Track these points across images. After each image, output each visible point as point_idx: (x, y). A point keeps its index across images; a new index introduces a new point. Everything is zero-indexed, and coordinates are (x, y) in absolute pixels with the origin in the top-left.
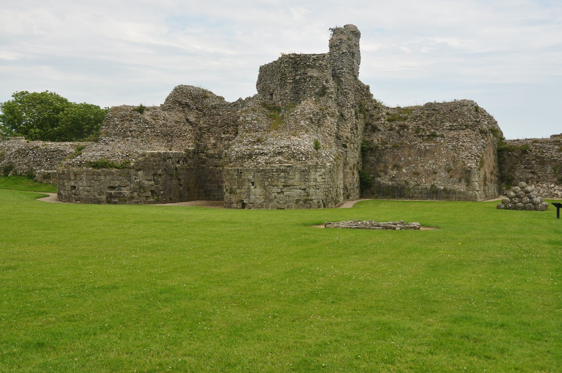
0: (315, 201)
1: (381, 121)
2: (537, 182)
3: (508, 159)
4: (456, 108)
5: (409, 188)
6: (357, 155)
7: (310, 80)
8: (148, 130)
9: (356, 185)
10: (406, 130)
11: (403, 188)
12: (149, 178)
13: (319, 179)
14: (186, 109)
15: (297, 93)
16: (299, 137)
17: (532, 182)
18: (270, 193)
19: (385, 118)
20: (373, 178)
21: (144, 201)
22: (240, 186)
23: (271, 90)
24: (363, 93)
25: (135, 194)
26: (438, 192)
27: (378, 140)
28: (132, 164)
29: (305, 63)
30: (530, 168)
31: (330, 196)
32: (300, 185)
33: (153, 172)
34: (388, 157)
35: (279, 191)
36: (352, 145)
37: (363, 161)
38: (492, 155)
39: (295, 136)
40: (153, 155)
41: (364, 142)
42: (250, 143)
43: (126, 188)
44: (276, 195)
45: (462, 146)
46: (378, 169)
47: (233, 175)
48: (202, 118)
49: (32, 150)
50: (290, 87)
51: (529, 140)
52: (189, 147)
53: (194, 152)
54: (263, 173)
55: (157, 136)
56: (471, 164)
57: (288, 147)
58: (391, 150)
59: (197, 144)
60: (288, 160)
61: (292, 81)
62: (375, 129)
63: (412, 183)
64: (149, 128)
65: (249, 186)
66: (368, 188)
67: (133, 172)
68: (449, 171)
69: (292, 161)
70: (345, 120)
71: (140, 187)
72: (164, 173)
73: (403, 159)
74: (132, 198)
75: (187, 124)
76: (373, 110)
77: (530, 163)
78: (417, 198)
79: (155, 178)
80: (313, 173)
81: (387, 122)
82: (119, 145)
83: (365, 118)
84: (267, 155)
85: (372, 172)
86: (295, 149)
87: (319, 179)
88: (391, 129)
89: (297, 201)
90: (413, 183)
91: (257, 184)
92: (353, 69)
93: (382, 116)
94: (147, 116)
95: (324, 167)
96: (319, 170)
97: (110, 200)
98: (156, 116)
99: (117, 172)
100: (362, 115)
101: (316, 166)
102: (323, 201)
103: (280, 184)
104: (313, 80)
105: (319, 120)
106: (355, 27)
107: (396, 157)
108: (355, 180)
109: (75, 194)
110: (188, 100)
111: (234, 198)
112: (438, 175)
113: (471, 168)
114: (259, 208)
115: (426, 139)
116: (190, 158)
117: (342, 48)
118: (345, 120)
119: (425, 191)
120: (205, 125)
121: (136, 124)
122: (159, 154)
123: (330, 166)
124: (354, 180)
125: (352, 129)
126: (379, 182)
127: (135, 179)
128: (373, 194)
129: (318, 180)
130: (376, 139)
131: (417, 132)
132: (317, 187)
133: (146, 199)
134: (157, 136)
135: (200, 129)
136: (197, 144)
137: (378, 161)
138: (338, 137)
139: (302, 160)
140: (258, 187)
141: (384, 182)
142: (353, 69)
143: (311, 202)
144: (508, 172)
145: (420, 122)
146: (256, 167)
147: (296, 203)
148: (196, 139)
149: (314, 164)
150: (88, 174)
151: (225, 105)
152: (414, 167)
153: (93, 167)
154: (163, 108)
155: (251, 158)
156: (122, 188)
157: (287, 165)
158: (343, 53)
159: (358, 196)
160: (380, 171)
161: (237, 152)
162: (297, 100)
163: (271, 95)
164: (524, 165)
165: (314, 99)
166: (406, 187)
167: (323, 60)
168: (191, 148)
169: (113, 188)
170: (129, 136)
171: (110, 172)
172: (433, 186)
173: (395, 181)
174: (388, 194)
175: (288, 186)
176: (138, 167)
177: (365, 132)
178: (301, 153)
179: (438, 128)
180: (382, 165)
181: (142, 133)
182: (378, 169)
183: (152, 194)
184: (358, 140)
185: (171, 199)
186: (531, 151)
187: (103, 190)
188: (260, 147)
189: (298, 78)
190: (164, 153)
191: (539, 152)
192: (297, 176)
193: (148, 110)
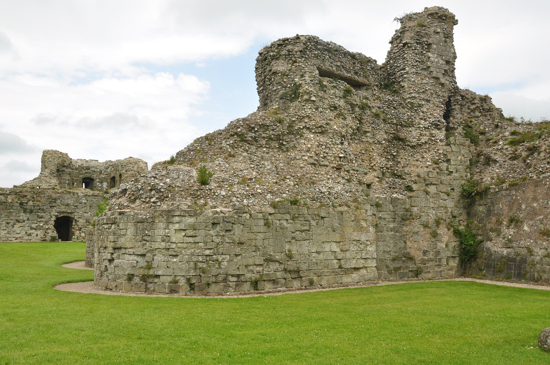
5: (533, 261)
10: (536, 155)
11: (524, 261)
20: (482, 241)
34: (502, 206)
46: (489, 226)
58: (508, 192)
66: (470, 257)
73: (523, 206)
76: (493, 131)
89: (130, 277)
90: (541, 252)
104: (278, 78)
107: (513, 204)
126: (488, 249)
141: (496, 249)
143: (156, 280)
152: (541, 221)
160: (491, 230)
166: (529, 259)
173: (512, 247)
174: (500, 271)
180: (494, 219)
182: (489, 226)
192: (131, 231)
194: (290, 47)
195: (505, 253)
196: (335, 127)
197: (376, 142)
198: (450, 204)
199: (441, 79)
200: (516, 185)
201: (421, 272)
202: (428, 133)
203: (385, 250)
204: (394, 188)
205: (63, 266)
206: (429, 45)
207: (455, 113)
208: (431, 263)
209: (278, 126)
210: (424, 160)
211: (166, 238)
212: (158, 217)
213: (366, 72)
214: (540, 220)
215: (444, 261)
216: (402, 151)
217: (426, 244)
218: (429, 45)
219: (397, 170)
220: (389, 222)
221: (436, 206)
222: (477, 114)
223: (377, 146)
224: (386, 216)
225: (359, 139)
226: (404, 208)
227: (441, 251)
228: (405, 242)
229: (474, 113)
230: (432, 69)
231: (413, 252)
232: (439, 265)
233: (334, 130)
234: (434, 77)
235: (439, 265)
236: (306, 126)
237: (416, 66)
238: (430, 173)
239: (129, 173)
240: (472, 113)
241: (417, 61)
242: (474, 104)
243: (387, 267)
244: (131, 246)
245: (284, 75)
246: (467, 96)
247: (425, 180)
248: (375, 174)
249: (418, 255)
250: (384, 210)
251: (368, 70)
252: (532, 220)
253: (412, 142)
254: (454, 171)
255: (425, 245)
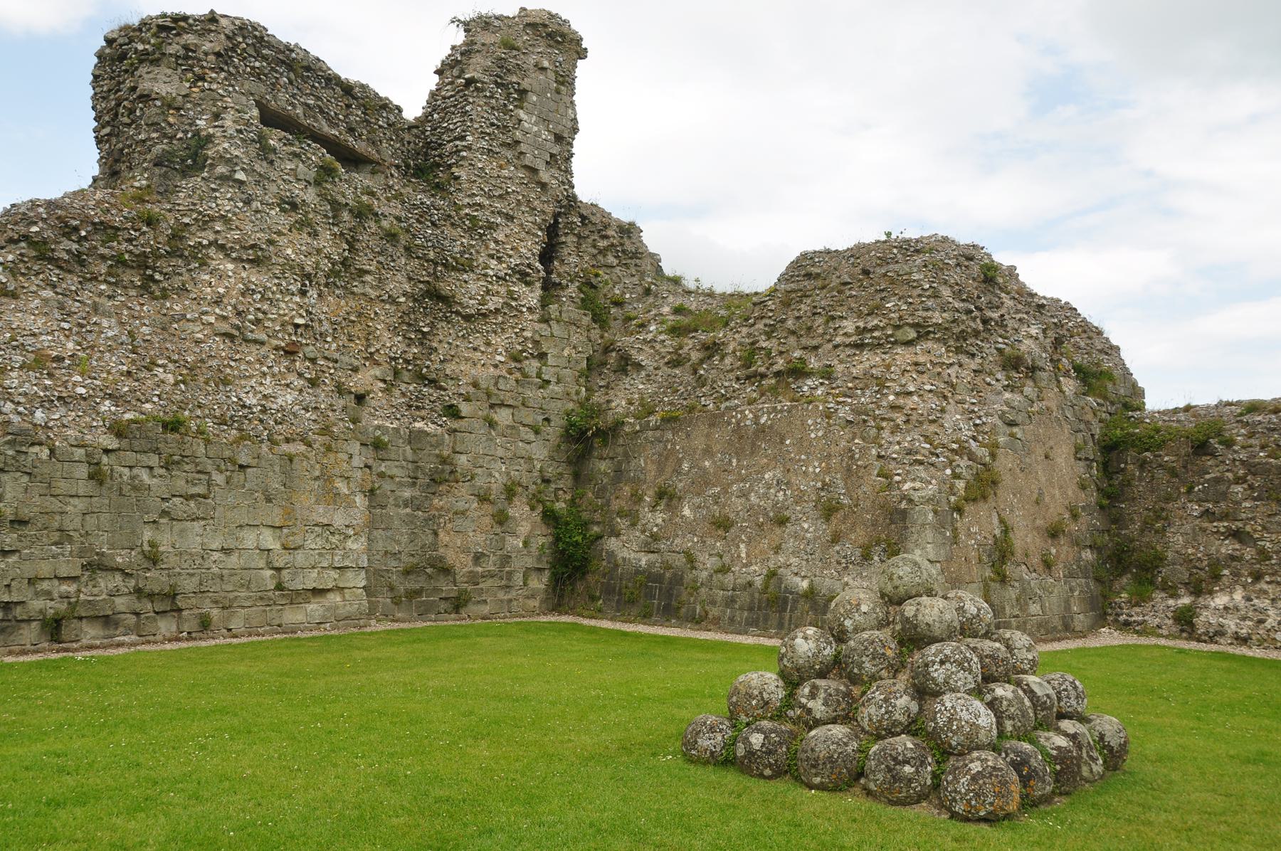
2: (1258, 577)
3: (1140, 479)
4: (884, 261)
11: (678, 580)
17: (1236, 574)
26: (785, 600)
30: (1225, 517)
34: (644, 463)
38: (1063, 455)
45: (893, 407)
51: (1229, 404)
56: (920, 486)
58: (658, 433)
66: (573, 571)
68: (829, 511)
73: (686, 466)
77: (1224, 496)
90: (711, 562)
104: (152, 112)
112: (790, 528)
113: (910, 501)
115: (773, 389)
119: (744, 598)
126: (611, 554)
130: (621, 400)
131: (748, 363)
141: (626, 555)
144: (1142, 531)
164: (1200, 501)
166: (688, 577)
172: (772, 574)
179: (815, 343)
180: (627, 490)
186: (1229, 444)
191: (1263, 447)
194: (190, 39)
195: (643, 563)
196: (289, 251)
197: (386, 297)
198: (539, 452)
199: (541, 174)
201: (467, 602)
202: (503, 290)
203: (389, 549)
204: (418, 408)
206: (523, 93)
207: (565, 251)
208: (490, 582)
209: (144, 233)
210: (490, 350)
213: (374, 131)
215: (518, 579)
216: (444, 324)
217: (480, 538)
218: (523, 93)
219: (428, 367)
220: (401, 484)
221: (510, 454)
222: (611, 259)
223: (387, 306)
224: (395, 471)
225: (345, 288)
226: (437, 456)
227: (513, 555)
228: (436, 534)
229: (605, 256)
230: (523, 147)
231: (451, 557)
232: (508, 587)
233: (287, 258)
234: (526, 167)
235: (508, 587)
236: (216, 241)
237: (489, 134)
238: (501, 380)
240: (600, 257)
241: (493, 125)
242: (606, 237)
243: (392, 589)
246: (593, 219)
247: (489, 395)
248: (377, 372)
249: (462, 564)
250: (393, 456)
251: (380, 127)
253: (468, 307)
254: (553, 380)
255: (478, 540)
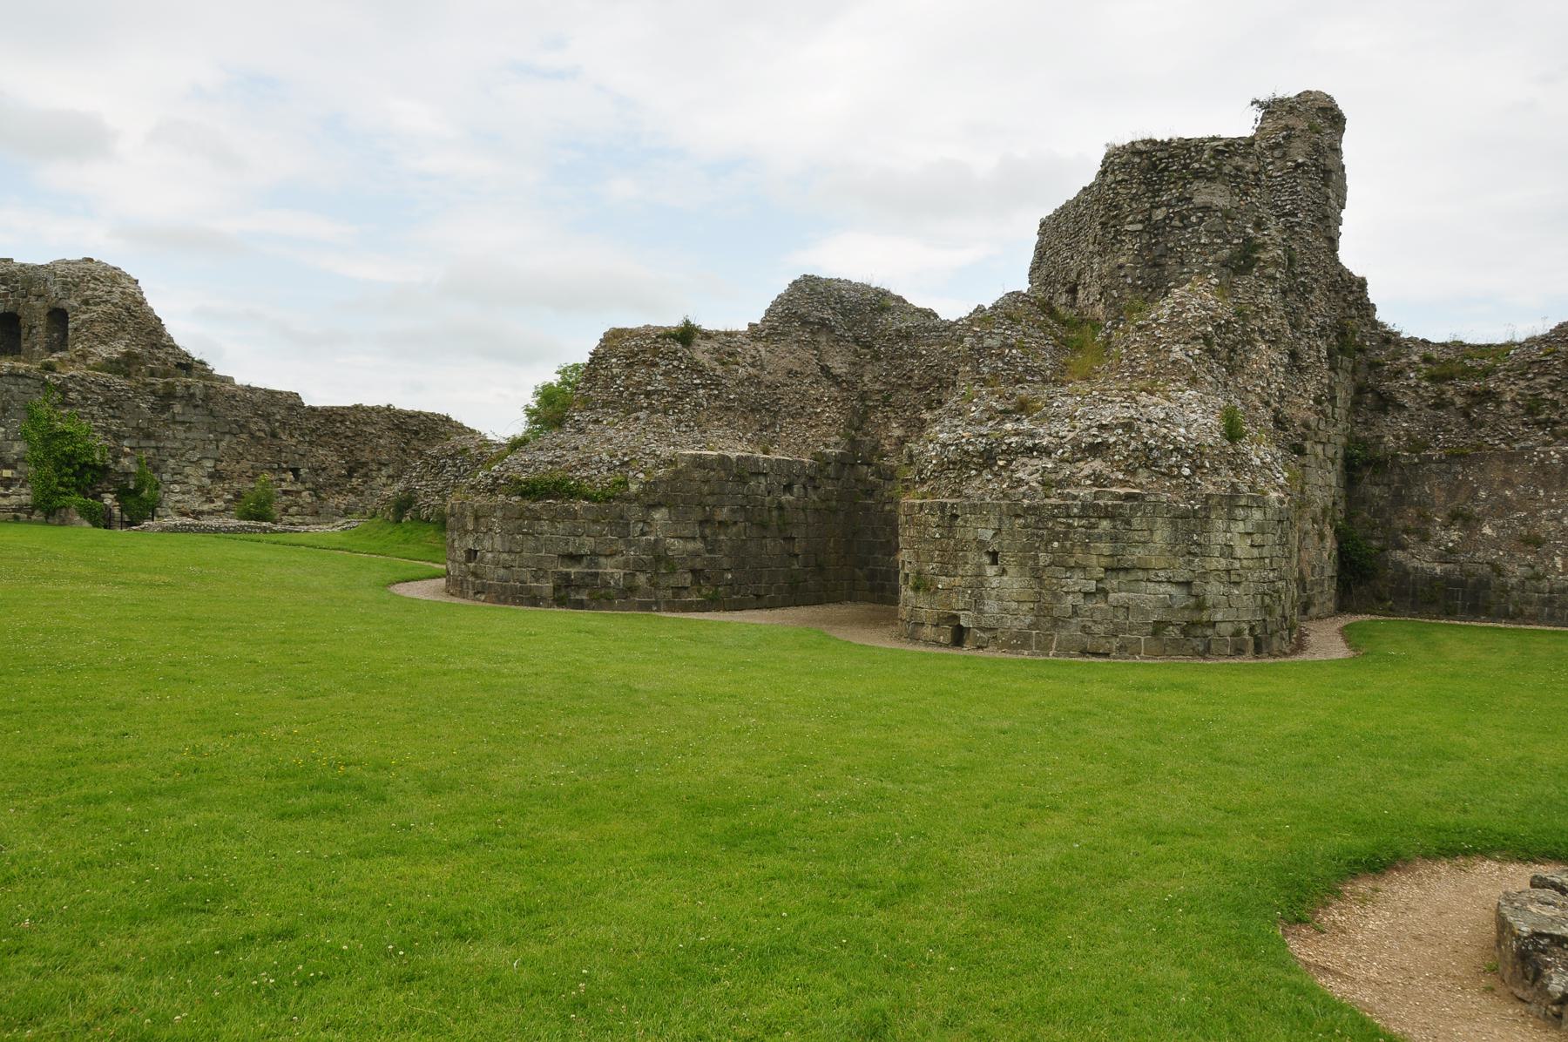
0: (1226, 629)
1: (1408, 378)
5: (1504, 585)
6: (1333, 479)
7: (1201, 220)
8: (701, 391)
9: (1329, 571)
10: (1490, 406)
11: (1483, 584)
12: (686, 533)
13: (1242, 548)
14: (823, 339)
15: (1156, 265)
16: (1168, 399)
18: (1055, 594)
19: (1419, 370)
20: (1383, 550)
21: (667, 603)
22: (950, 560)
23: (1074, 275)
24: (1350, 298)
25: (641, 579)
27: (1398, 438)
28: (634, 488)
29: (1186, 166)
31: (1279, 611)
32: (1171, 567)
33: (697, 514)
34: (1432, 489)
35: (1092, 586)
36: (1319, 448)
37: (1349, 499)
39: (1152, 393)
40: (699, 463)
41: (1353, 441)
42: (992, 414)
43: (611, 561)
44: (1080, 600)
47: (926, 525)
48: (869, 367)
49: (452, 457)
50: (1131, 245)
52: (827, 446)
53: (842, 462)
54: (1031, 520)
55: (728, 409)
57: (1128, 426)
58: (1444, 466)
59: (852, 440)
60: (1126, 472)
61: (1140, 227)
62: (1385, 403)
63: (1516, 572)
64: (704, 387)
65: (980, 566)
66: (1364, 580)
67: (635, 511)
69: (1143, 476)
70: (1300, 370)
71: (658, 559)
72: (740, 517)
73: (1483, 494)
74: (631, 590)
75: (825, 382)
78: (1534, 618)
79: (707, 531)
80: (1220, 524)
81: (1425, 384)
82: (611, 433)
83: (1354, 372)
84: (1049, 455)
85: (1377, 533)
86: (1153, 434)
87: (1242, 548)
88: (1441, 404)
89: (1159, 628)
90: (1520, 571)
91: (1008, 559)
92: (1327, 217)
93: (1410, 365)
94: (701, 353)
95: (1260, 502)
96: (1240, 513)
97: (565, 595)
98: (730, 355)
99: (587, 509)
100: (1347, 363)
101: (1231, 500)
102: (1252, 629)
103: (1094, 560)
104: (1213, 221)
105: (1233, 350)
106: (1331, 100)
107: (1458, 487)
108: (1325, 555)
109: (474, 574)
110: (836, 322)
111: (926, 608)
114: (1015, 647)
116: (828, 477)
117: (1292, 151)
118: (1300, 370)
120: (877, 387)
121: (665, 374)
122: (723, 460)
123: (1281, 502)
124: (1321, 554)
125: (1318, 401)
126: (1398, 564)
127: (643, 534)
128: (1381, 600)
129: (1238, 553)
130: (1392, 433)
132: (1231, 578)
133: (675, 595)
134: (728, 409)
135: (863, 397)
136: (852, 440)
137: (1399, 500)
138: (1280, 422)
139: (1180, 475)
140: (1011, 570)
141: (1416, 563)
142: (1327, 217)
143: (1209, 632)
145: (1544, 380)
146: (1006, 496)
147: (1154, 634)
148: (850, 425)
149: (1225, 490)
150: (509, 515)
151: (936, 328)
152: (1523, 521)
153: (524, 494)
154: (754, 333)
155: (990, 467)
156: (602, 560)
157: (1122, 491)
158: (1298, 166)
159: (1331, 605)
160: (1406, 531)
161: (944, 445)
162: (1156, 287)
163: (1073, 291)
165: (1215, 281)
166: (1496, 581)
167: (1245, 156)
168: (833, 451)
169: (574, 558)
170: (642, 408)
171: (566, 510)
175: (1127, 570)
176: (654, 498)
177: (1357, 413)
178: (1177, 449)
180: (1412, 512)
181: (681, 399)
182: (1399, 524)
183: (696, 582)
184: (1336, 435)
185: (758, 596)
187: (546, 565)
188: (1026, 425)
189: (1159, 214)
190: (739, 458)
192: (1162, 535)
193: (708, 336)
194: (1238, 160)
195: (1438, 570)
200: (1465, 455)
205: (402, 590)
211: (1228, 551)
212: (1215, 507)
214: (1519, 519)
239: (99, 309)
244: (1163, 565)
245: (1228, 217)
252: (1500, 517)
